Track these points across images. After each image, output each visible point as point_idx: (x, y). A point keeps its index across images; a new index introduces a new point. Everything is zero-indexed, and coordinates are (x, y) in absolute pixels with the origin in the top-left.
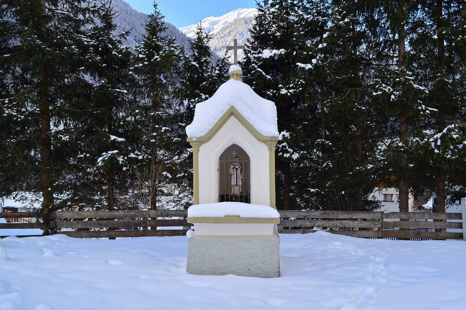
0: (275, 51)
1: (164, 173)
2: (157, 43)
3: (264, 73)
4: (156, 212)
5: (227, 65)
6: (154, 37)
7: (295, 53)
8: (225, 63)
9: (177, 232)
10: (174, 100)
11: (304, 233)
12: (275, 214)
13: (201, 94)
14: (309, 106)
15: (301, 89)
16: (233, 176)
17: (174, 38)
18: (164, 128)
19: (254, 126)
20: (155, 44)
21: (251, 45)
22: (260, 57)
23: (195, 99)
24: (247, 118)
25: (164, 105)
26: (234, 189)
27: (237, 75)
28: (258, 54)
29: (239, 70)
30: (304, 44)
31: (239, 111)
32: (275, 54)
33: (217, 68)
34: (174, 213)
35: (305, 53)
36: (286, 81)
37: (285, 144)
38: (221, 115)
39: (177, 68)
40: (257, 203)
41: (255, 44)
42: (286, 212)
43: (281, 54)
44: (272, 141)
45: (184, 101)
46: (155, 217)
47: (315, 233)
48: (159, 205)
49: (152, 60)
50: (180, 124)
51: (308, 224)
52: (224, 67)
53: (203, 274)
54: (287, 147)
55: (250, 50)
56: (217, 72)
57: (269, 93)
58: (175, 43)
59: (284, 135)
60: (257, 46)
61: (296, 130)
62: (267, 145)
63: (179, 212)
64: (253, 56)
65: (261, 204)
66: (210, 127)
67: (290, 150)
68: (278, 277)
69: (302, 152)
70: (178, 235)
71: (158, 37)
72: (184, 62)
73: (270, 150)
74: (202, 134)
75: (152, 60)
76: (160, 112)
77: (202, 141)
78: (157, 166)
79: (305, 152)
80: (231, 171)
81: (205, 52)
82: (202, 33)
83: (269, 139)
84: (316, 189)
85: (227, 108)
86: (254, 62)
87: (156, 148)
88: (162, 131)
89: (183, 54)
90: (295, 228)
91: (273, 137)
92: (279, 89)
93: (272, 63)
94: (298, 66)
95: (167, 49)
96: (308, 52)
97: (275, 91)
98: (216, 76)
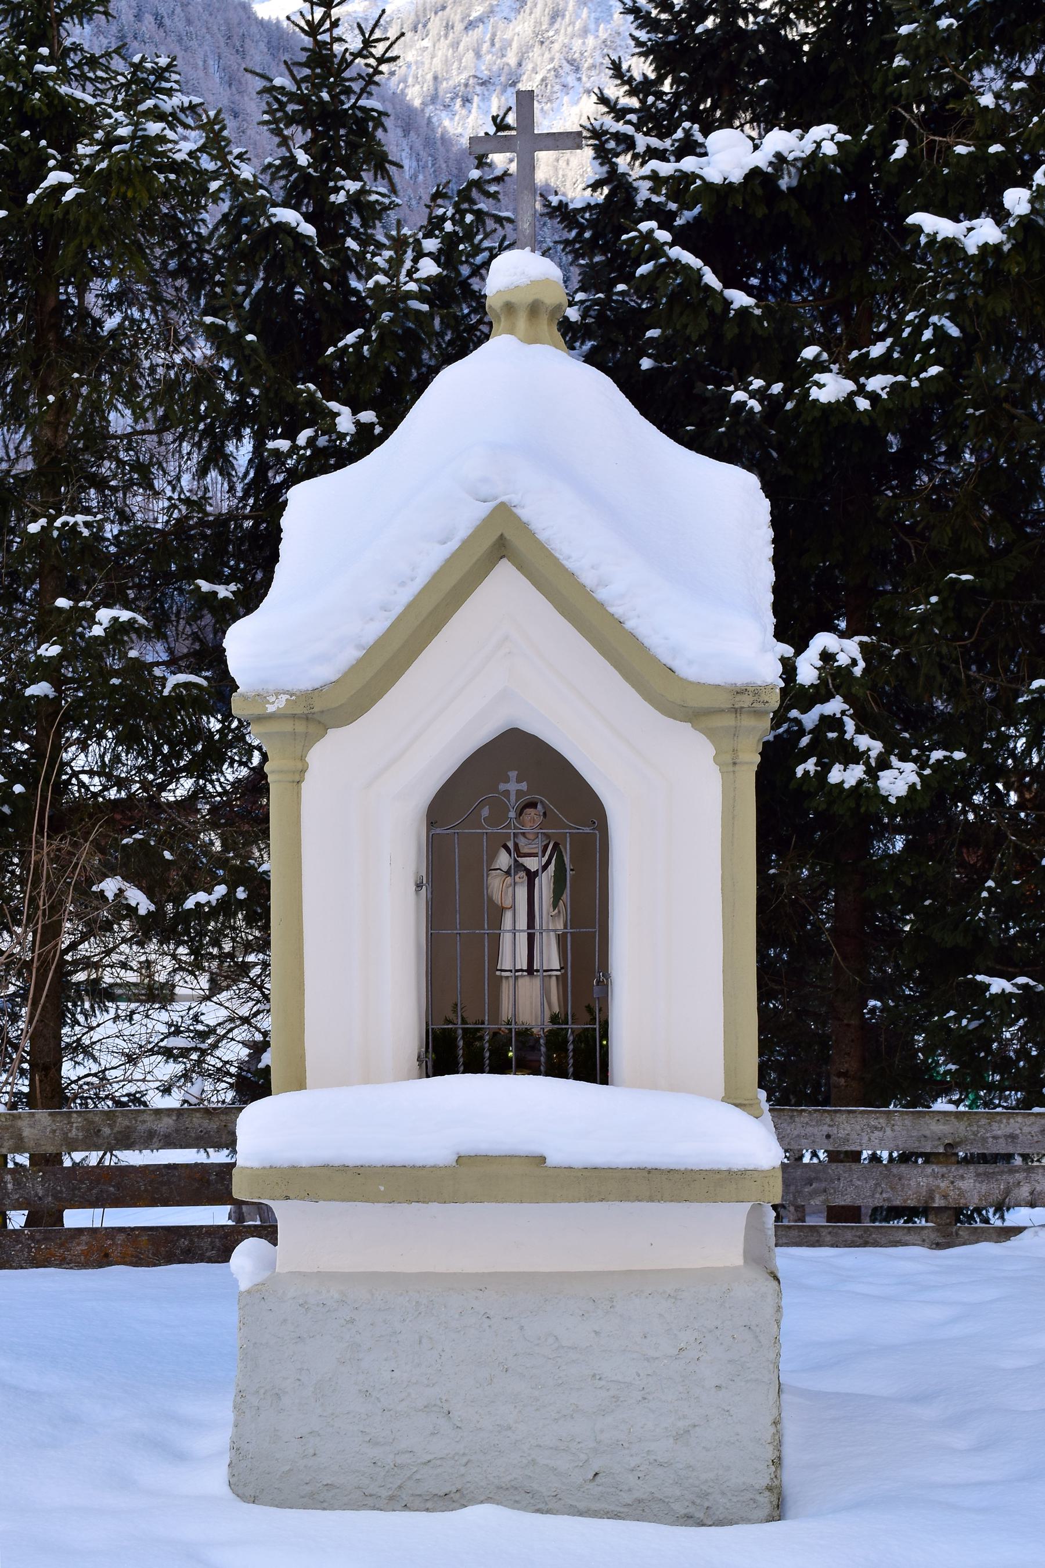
0: (780, 141)
1: (110, 886)
2: (64, 90)
3: (710, 278)
4: (60, 1123)
5: (490, 224)
6: (44, 51)
7: (901, 149)
8: (479, 214)
9: (184, 1243)
10: (169, 437)
11: (945, 1240)
12: (752, 1141)
13: (334, 406)
14: (987, 471)
15: (934, 370)
16: (508, 916)
17: (163, 61)
18: (104, 615)
19: (630, 625)
20: (51, 95)
21: (634, 103)
22: (693, 177)
23: (291, 434)
24: (588, 578)
25: (107, 467)
26: (512, 1008)
27: (534, 309)
28: (679, 156)
29: (546, 282)
30: (964, 91)
31: (542, 536)
32: (778, 155)
33: (431, 245)
34: (166, 1124)
35: (961, 150)
36: (847, 320)
37: (835, 706)
38: (431, 558)
39: (184, 245)
40: (650, 1082)
41: (659, 95)
42: (841, 1118)
43: (814, 156)
44: (736, 711)
45: (230, 447)
46: (51, 1149)
47: (1015, 1241)
48: (81, 1071)
49: (31, 198)
50: (205, 586)
51: (970, 1187)
52: (469, 235)
53: (324, 1505)
54: (850, 725)
55: (629, 130)
56: (428, 268)
57: (740, 396)
58: (169, 92)
59: (827, 657)
60: (674, 105)
61: (909, 619)
62: (711, 734)
63: (197, 1120)
64: (646, 170)
65: (677, 1085)
66: (374, 629)
67: (863, 742)
68: (770, 1519)
69: (937, 755)
70: (190, 1256)
71: (66, 52)
72: (225, 207)
73: (728, 765)
74: (325, 673)
75: (31, 198)
76: (80, 518)
77: (319, 713)
78: (66, 845)
79: (959, 755)
80: (496, 884)
81: (352, 146)
82: (335, 24)
83: (724, 701)
84: (1021, 980)
85: (468, 517)
86: (651, 211)
87: (59, 735)
88: (97, 631)
89: (221, 155)
90: (895, 1212)
91: (741, 691)
92: (800, 376)
93: (761, 211)
94: (918, 229)
95: (123, 132)
96: (982, 144)
97: (777, 388)
98: (421, 296)
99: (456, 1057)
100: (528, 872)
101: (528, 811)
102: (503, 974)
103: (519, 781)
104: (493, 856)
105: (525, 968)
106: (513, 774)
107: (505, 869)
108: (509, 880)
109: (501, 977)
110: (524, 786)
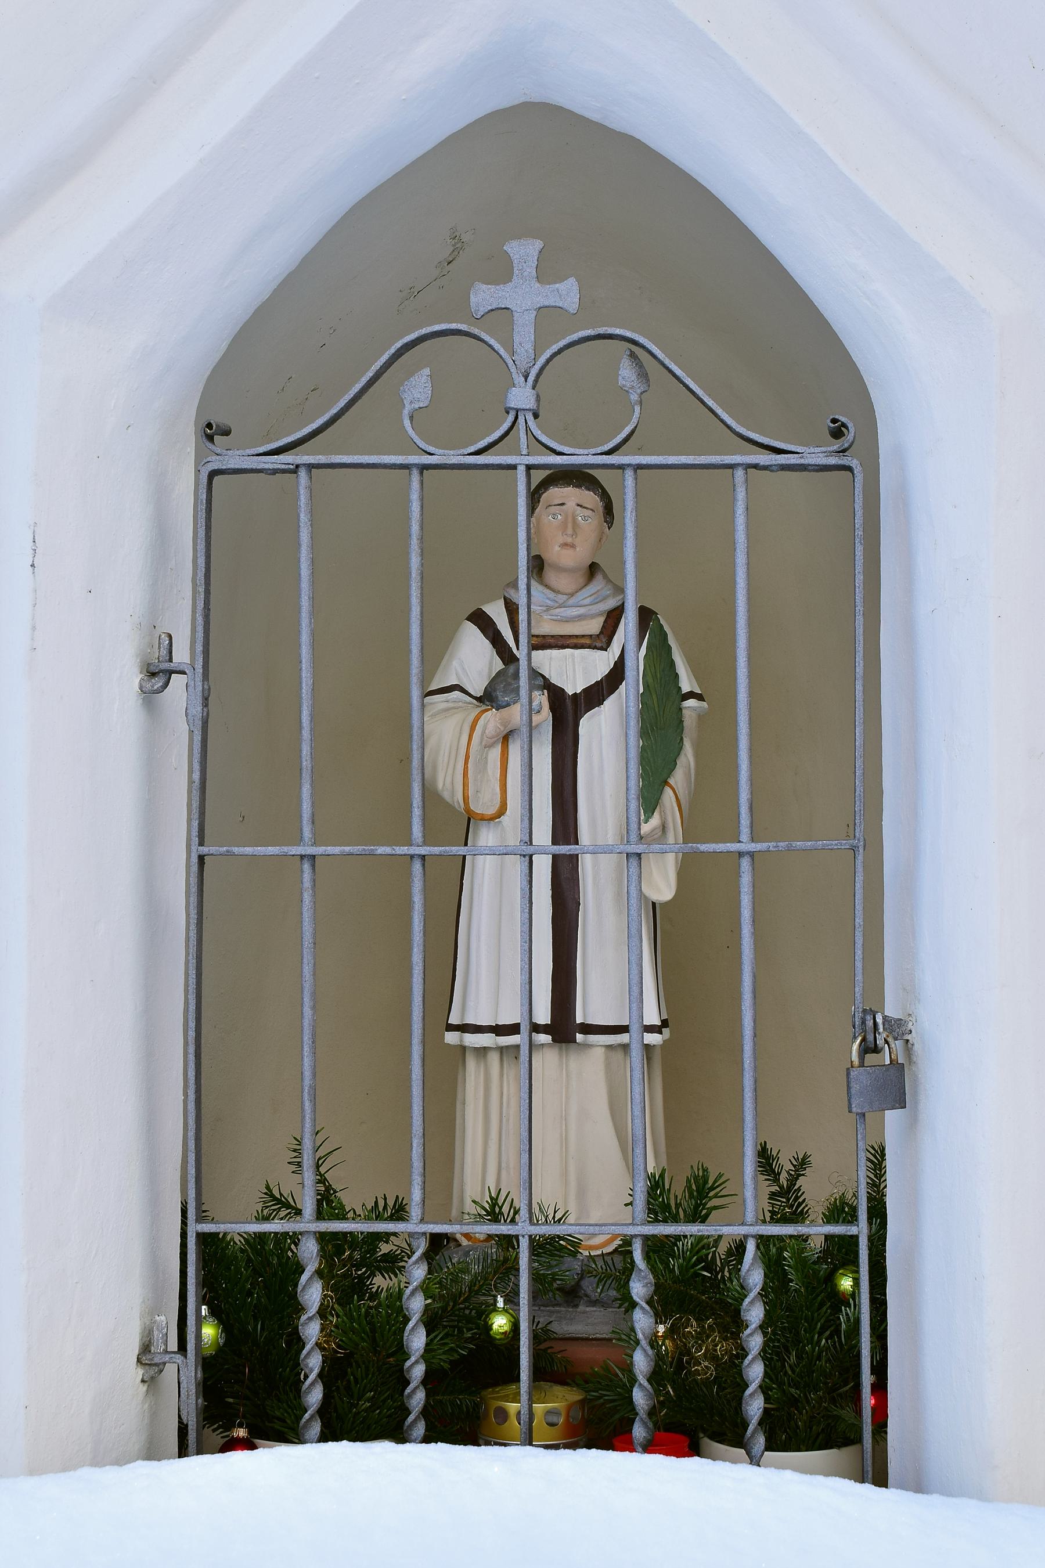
80: (447, 736)
99: (297, 1342)
100: (556, 694)
101: (555, 493)
102: (472, 1040)
103: (545, 274)
104: (437, 649)
105: (543, 1015)
106: (524, 252)
107: (478, 690)
108: (491, 720)
109: (463, 1049)
110: (567, 294)
